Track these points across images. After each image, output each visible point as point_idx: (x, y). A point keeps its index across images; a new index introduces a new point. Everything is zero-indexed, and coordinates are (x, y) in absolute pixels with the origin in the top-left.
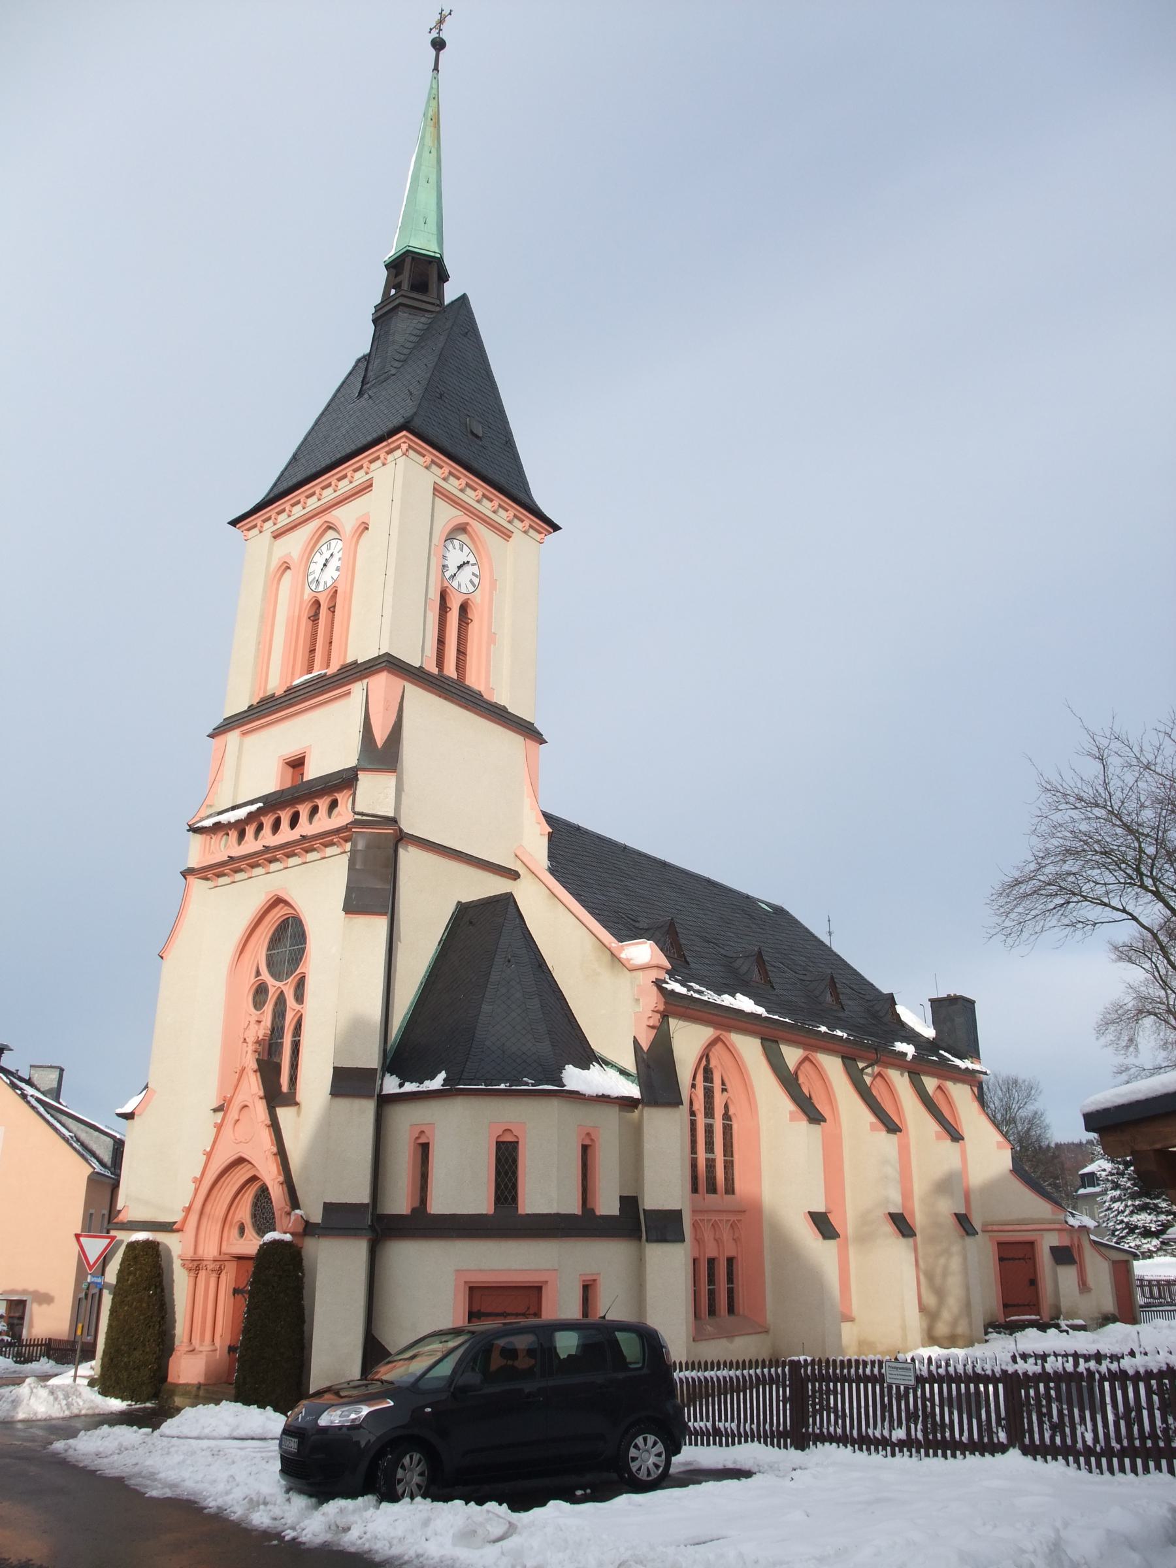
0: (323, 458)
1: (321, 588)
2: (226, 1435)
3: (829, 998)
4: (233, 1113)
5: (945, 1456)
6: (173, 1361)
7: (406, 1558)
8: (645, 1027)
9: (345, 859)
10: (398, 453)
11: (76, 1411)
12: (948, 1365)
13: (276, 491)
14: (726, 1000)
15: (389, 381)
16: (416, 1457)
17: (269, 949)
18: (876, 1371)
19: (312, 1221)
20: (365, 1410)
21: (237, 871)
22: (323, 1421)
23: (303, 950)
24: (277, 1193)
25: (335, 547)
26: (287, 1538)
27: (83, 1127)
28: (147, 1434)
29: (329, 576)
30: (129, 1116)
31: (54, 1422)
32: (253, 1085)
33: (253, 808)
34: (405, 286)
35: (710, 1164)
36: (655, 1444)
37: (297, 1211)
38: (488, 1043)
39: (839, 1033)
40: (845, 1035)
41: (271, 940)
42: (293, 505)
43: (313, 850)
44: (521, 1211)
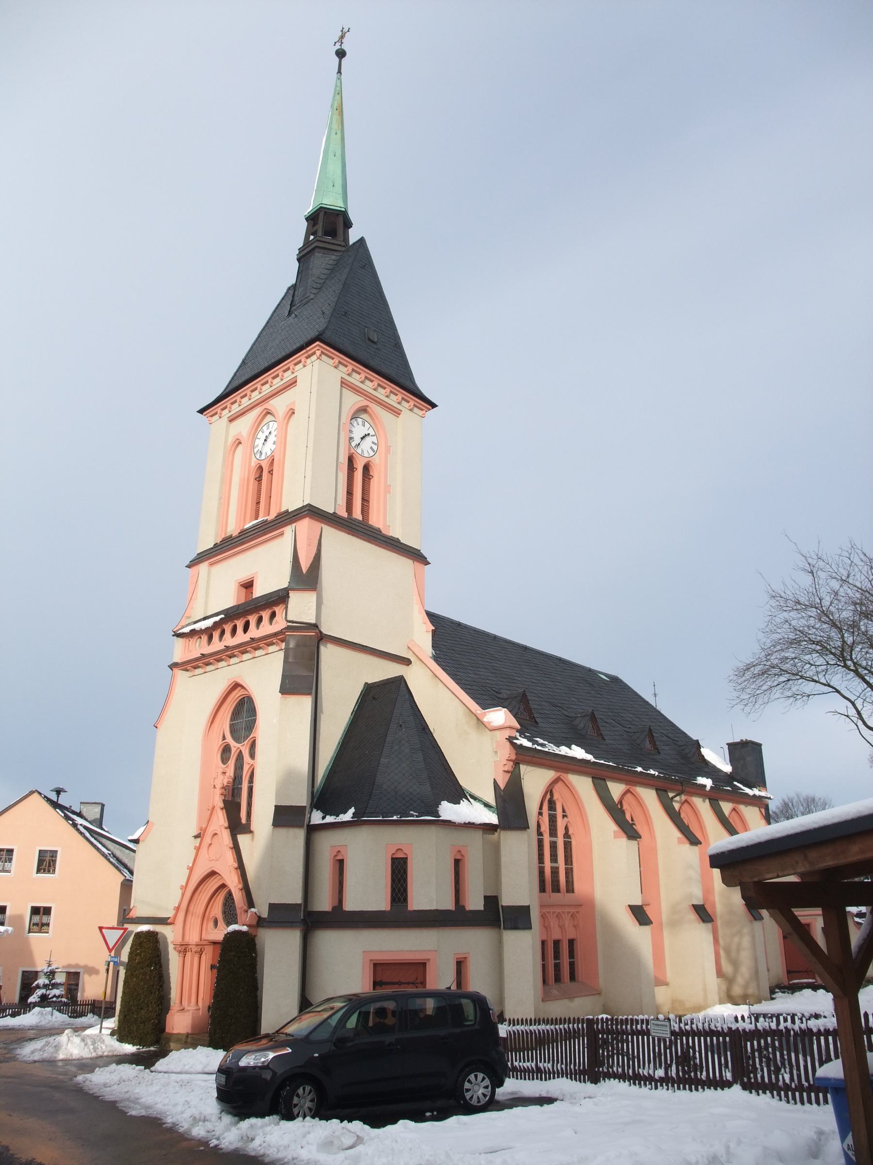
0: (260, 365)
1: (263, 457)
2: (200, 1070)
3: (648, 745)
4: (207, 839)
5: (691, 1090)
6: (169, 1017)
7: (286, 1160)
8: (501, 771)
9: (281, 654)
10: (314, 358)
11: (100, 1053)
12: (692, 1023)
13: (231, 388)
14: (563, 750)
15: (309, 304)
16: (308, 1088)
17: (231, 720)
18: (644, 1027)
19: (262, 916)
20: (271, 1055)
21: (207, 664)
22: (243, 1063)
23: (255, 720)
24: (238, 897)
25: (272, 427)
26: (211, 1145)
27: (118, 846)
28: (140, 1070)
29: (268, 449)
30: (136, 841)
31: (84, 1061)
32: (221, 819)
33: (217, 619)
34: (320, 233)
35: (555, 872)
36: (483, 1079)
37: (253, 910)
38: (385, 787)
39: (652, 772)
40: (657, 773)
41: (233, 713)
42: (242, 398)
43: (259, 648)
44: (410, 908)
